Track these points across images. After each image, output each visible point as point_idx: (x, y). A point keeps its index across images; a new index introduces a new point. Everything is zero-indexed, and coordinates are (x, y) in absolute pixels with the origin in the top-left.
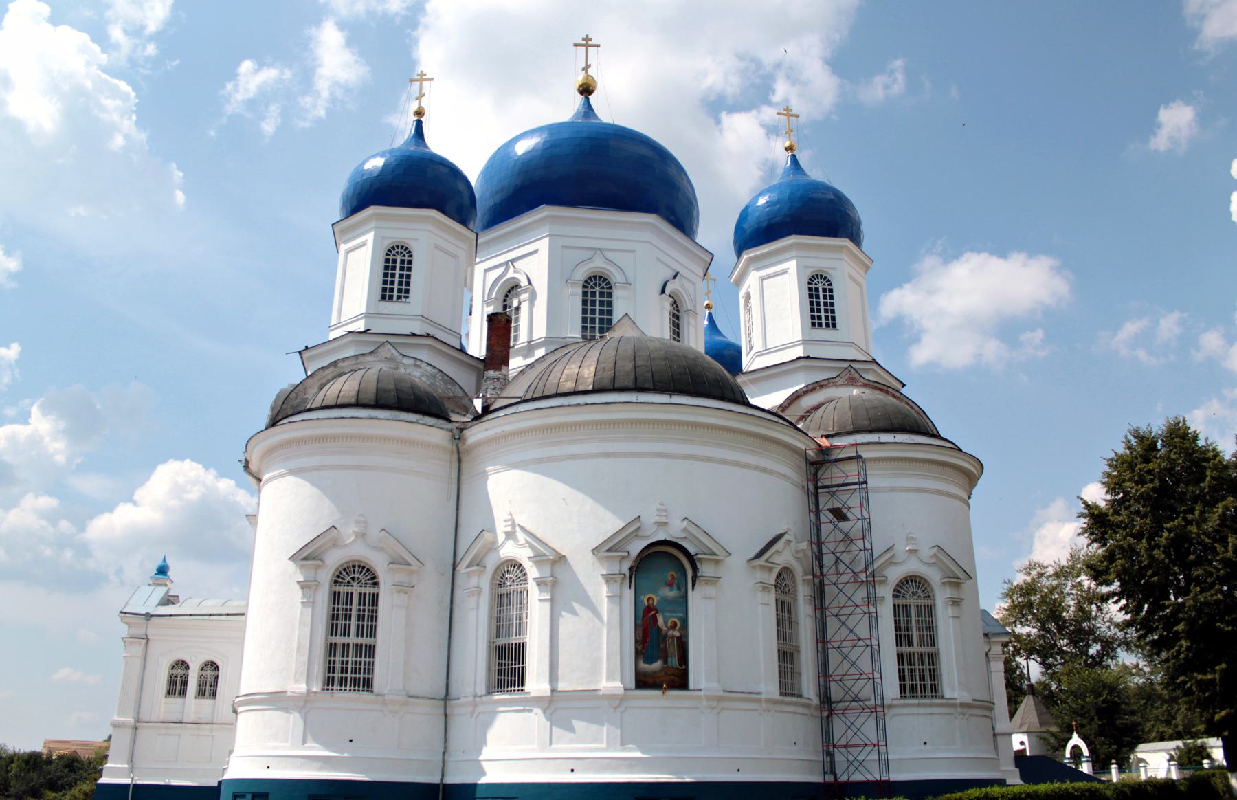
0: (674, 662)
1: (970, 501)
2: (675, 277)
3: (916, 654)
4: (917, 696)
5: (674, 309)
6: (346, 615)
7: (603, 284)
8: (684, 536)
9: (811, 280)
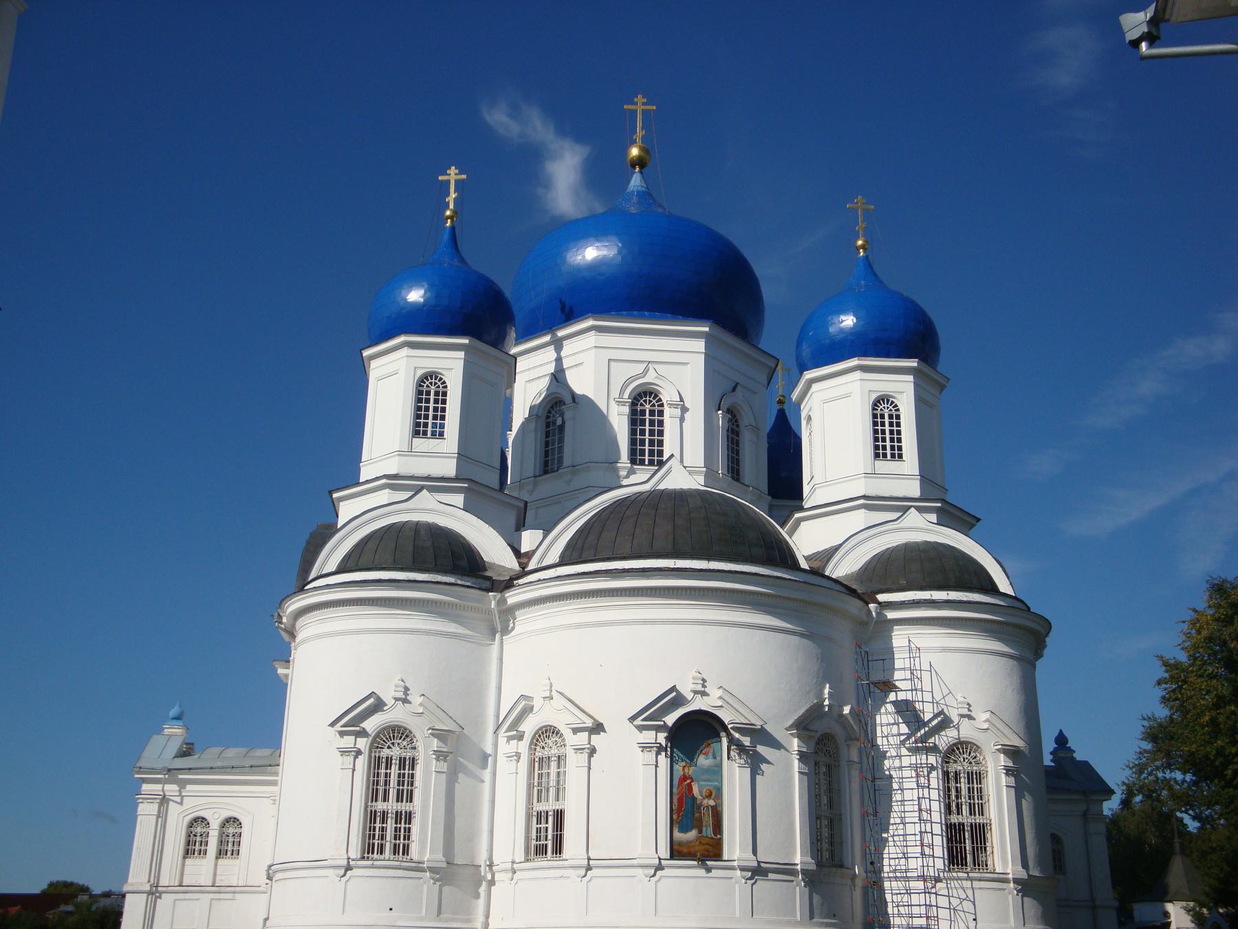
0: (709, 831)
2: (734, 389)
5: (733, 424)
7: (433, 381)
8: (720, 704)
9: (875, 404)
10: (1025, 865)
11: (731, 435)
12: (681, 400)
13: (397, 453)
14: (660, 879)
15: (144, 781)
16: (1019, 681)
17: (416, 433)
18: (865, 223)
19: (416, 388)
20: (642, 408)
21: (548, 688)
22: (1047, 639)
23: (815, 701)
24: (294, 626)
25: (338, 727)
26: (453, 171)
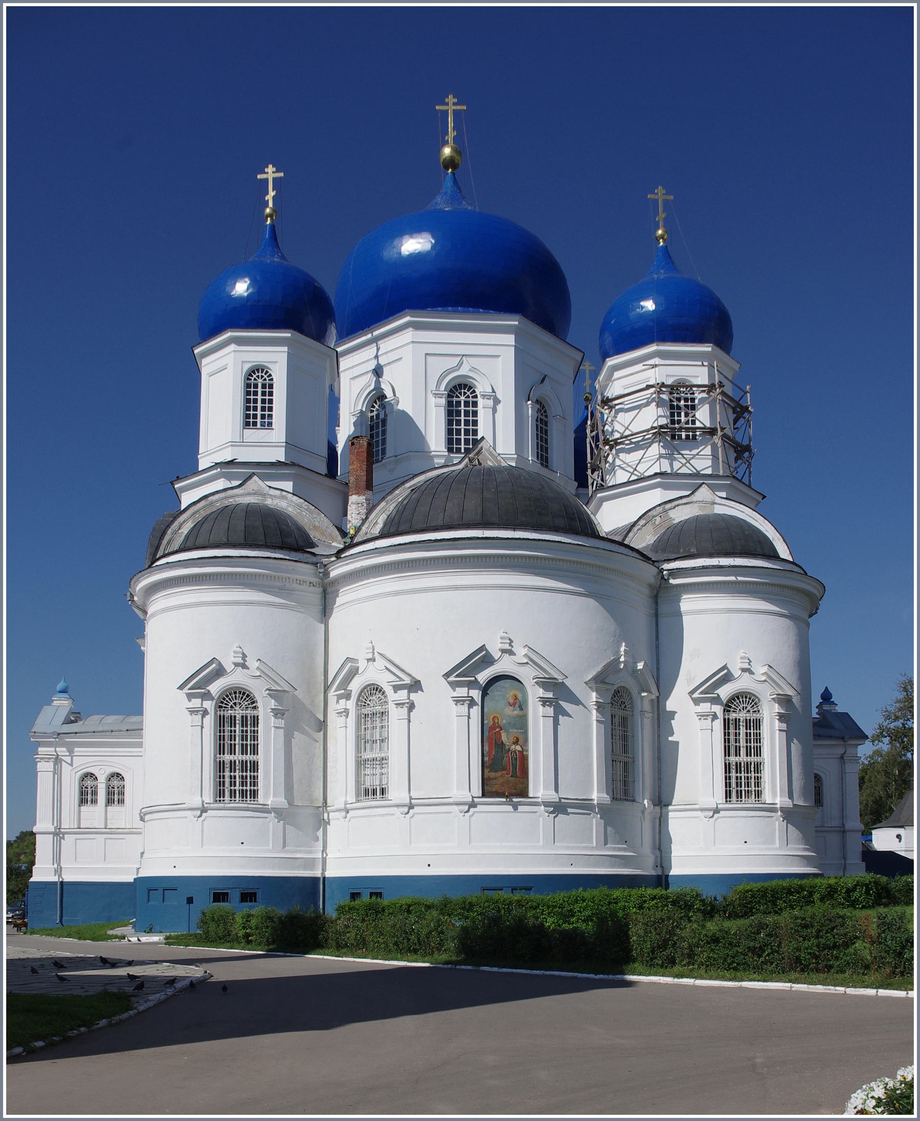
1: (810, 620)
3: (753, 763)
4: (246, 801)
5: (542, 414)
6: (231, 736)
7: (468, 393)
10: (791, 796)
11: (540, 425)
12: (494, 391)
13: (230, 444)
14: (472, 815)
15: (39, 744)
16: (794, 639)
17: (247, 424)
18: (665, 213)
19: (244, 381)
20: (458, 399)
21: (371, 651)
22: (820, 602)
23: (612, 658)
24: (145, 604)
25: (186, 690)
26: (270, 169)
